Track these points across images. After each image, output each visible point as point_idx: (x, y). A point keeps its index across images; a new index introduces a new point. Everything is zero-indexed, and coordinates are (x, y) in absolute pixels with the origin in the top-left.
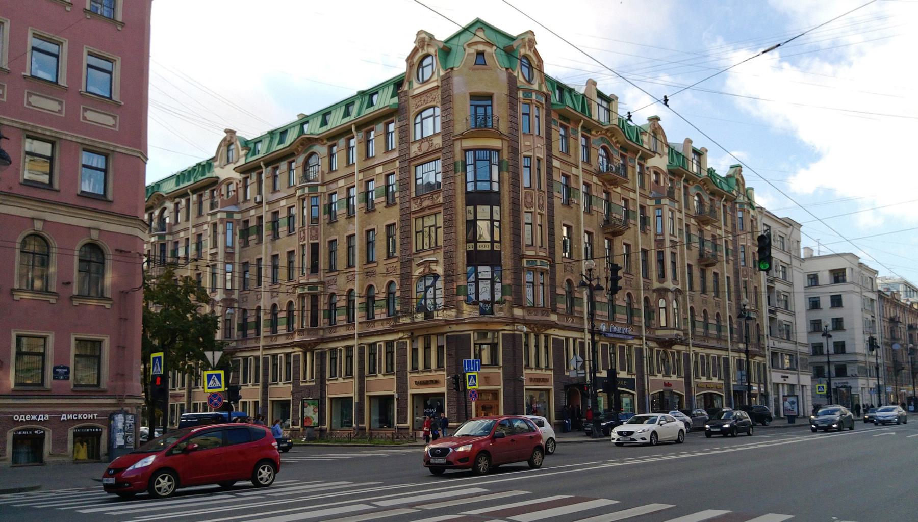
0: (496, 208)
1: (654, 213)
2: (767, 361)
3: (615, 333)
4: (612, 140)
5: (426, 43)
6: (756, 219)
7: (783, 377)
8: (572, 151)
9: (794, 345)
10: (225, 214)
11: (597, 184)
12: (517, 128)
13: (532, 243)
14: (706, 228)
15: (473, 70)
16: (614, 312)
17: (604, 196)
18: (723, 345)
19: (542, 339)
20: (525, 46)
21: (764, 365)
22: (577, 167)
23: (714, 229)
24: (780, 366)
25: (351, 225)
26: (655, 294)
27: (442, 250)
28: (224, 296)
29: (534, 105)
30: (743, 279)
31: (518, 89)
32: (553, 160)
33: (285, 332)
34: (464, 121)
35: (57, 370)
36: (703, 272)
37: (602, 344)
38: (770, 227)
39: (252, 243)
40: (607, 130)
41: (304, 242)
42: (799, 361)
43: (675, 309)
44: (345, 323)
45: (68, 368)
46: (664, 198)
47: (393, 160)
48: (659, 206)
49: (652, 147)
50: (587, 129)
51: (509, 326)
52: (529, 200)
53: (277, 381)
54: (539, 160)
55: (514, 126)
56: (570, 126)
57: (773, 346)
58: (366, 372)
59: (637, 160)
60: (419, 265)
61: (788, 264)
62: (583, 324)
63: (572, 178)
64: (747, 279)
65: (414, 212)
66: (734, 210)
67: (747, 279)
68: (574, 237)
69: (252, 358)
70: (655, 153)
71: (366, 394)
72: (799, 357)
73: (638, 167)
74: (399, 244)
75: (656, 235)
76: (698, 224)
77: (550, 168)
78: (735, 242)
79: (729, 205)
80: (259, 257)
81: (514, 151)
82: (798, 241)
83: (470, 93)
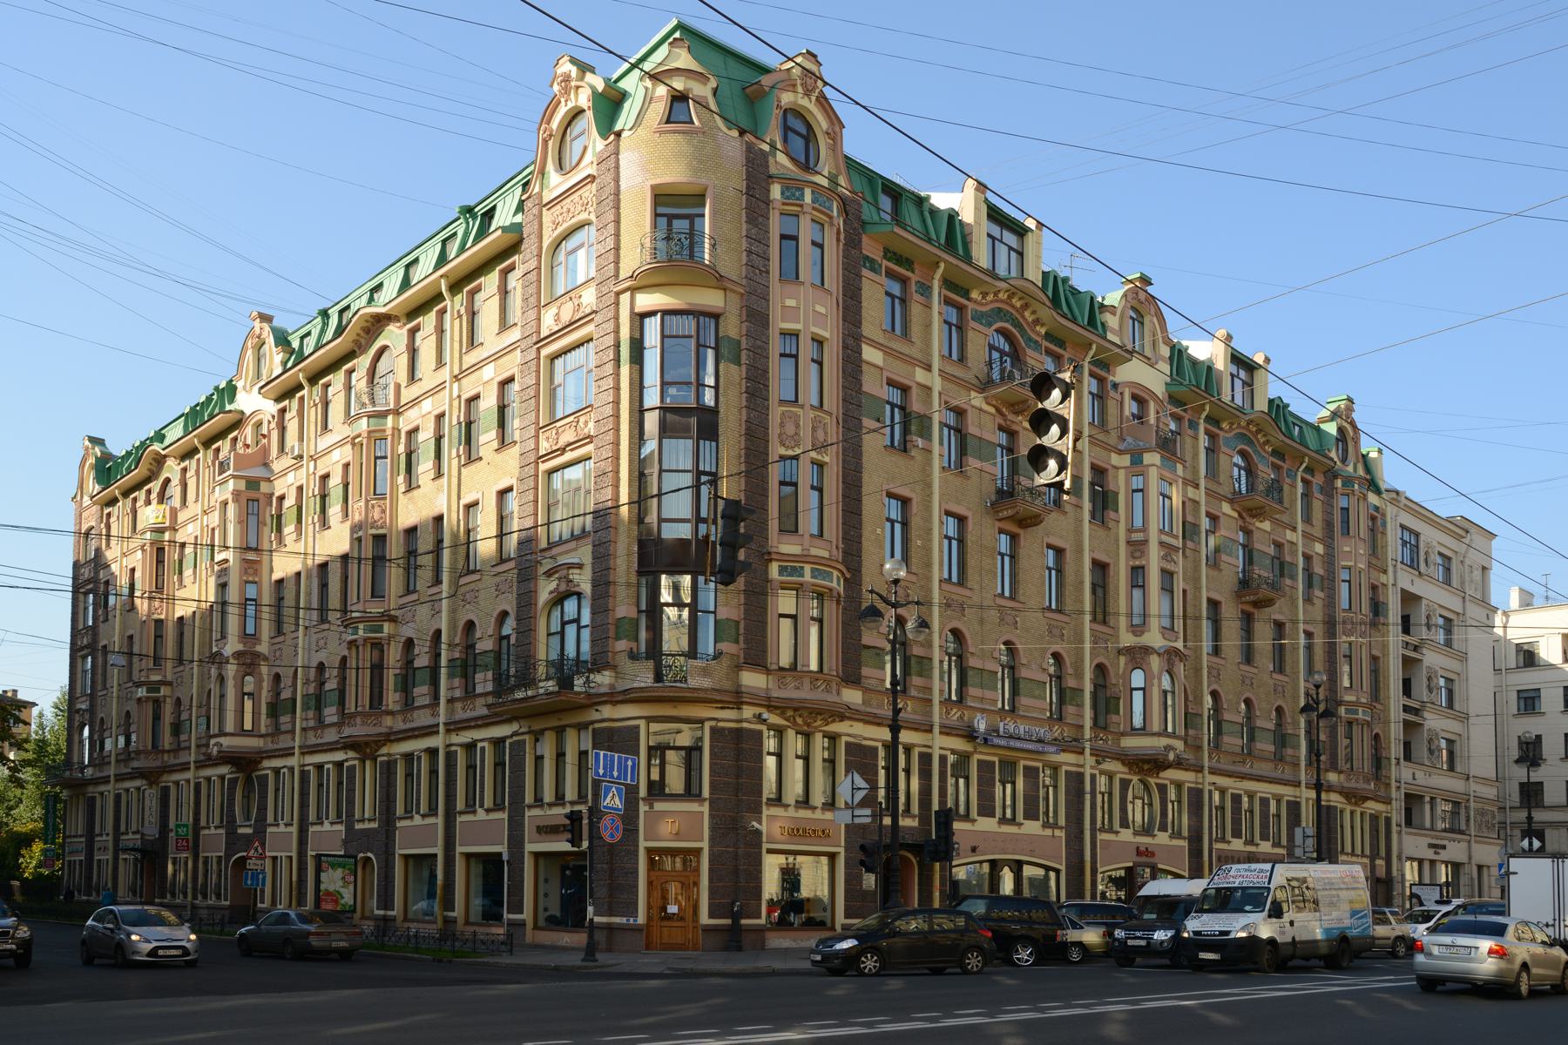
0: (706, 446)
1: (1127, 482)
2: (1394, 812)
3: (1011, 737)
4: (1023, 317)
6: (1384, 515)
7: (1431, 846)
8: (916, 330)
9: (1463, 782)
10: (244, 481)
11: (981, 410)
12: (766, 266)
13: (1351, 684)
15: (661, 133)
16: (1252, 739)
17: (1241, 537)
18: (1287, 773)
19: (819, 742)
20: (794, 86)
21: (1388, 820)
22: (928, 368)
23: (1281, 529)
24: (1428, 824)
26: (1122, 660)
27: (590, 540)
28: (240, 647)
29: (808, 218)
30: (1344, 638)
31: (771, 178)
33: (335, 719)
36: (1248, 620)
37: (978, 760)
38: (1417, 535)
40: (1250, 422)
41: (360, 533)
42: (1472, 813)
43: (1165, 692)
46: (1149, 450)
48: (1138, 469)
49: (1126, 342)
50: (956, 287)
51: (727, 711)
52: (790, 429)
54: (819, 342)
55: (757, 261)
56: (914, 278)
57: (1411, 781)
58: (460, 804)
59: (1299, 474)
60: (549, 574)
61: (1458, 614)
62: (930, 714)
63: (915, 393)
64: (1353, 639)
66: (1328, 491)
67: (1353, 639)
68: (916, 521)
69: (285, 770)
70: (1131, 353)
71: (459, 849)
72: (1472, 804)
73: (1300, 484)
75: (1130, 530)
76: (1240, 515)
77: (852, 365)
78: (1330, 558)
79: (1318, 480)
81: (757, 317)
82: (1484, 568)
83: (653, 187)
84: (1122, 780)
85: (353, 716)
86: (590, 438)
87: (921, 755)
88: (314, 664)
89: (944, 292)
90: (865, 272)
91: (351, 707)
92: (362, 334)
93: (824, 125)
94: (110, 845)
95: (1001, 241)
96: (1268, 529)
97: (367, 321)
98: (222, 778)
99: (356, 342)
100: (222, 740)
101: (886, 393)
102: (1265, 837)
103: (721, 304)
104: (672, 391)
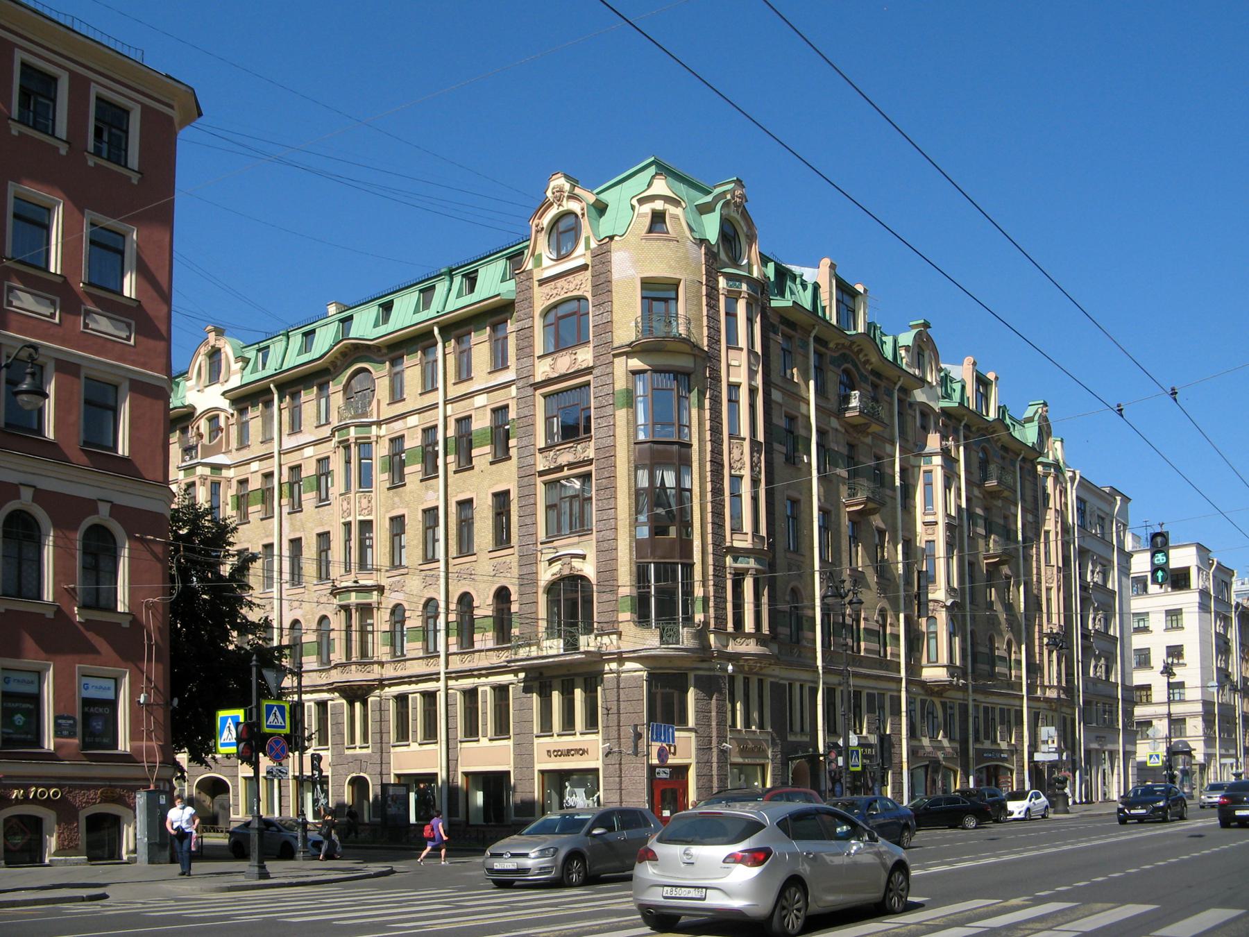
4: (858, 358)
5: (566, 194)
11: (837, 430)
14: (995, 503)
25: (430, 492)
32: (773, 390)
35: (60, 721)
41: (348, 519)
44: (421, 654)
45: (74, 719)
47: (507, 385)
53: (408, 740)
60: (551, 561)
65: (541, 474)
71: (461, 769)
74: (517, 526)
76: (984, 497)
80: (266, 541)
86: (590, 462)
87: (810, 688)
93: (745, 229)
95: (843, 302)
96: (1000, 505)
99: (333, 363)
102: (987, 737)
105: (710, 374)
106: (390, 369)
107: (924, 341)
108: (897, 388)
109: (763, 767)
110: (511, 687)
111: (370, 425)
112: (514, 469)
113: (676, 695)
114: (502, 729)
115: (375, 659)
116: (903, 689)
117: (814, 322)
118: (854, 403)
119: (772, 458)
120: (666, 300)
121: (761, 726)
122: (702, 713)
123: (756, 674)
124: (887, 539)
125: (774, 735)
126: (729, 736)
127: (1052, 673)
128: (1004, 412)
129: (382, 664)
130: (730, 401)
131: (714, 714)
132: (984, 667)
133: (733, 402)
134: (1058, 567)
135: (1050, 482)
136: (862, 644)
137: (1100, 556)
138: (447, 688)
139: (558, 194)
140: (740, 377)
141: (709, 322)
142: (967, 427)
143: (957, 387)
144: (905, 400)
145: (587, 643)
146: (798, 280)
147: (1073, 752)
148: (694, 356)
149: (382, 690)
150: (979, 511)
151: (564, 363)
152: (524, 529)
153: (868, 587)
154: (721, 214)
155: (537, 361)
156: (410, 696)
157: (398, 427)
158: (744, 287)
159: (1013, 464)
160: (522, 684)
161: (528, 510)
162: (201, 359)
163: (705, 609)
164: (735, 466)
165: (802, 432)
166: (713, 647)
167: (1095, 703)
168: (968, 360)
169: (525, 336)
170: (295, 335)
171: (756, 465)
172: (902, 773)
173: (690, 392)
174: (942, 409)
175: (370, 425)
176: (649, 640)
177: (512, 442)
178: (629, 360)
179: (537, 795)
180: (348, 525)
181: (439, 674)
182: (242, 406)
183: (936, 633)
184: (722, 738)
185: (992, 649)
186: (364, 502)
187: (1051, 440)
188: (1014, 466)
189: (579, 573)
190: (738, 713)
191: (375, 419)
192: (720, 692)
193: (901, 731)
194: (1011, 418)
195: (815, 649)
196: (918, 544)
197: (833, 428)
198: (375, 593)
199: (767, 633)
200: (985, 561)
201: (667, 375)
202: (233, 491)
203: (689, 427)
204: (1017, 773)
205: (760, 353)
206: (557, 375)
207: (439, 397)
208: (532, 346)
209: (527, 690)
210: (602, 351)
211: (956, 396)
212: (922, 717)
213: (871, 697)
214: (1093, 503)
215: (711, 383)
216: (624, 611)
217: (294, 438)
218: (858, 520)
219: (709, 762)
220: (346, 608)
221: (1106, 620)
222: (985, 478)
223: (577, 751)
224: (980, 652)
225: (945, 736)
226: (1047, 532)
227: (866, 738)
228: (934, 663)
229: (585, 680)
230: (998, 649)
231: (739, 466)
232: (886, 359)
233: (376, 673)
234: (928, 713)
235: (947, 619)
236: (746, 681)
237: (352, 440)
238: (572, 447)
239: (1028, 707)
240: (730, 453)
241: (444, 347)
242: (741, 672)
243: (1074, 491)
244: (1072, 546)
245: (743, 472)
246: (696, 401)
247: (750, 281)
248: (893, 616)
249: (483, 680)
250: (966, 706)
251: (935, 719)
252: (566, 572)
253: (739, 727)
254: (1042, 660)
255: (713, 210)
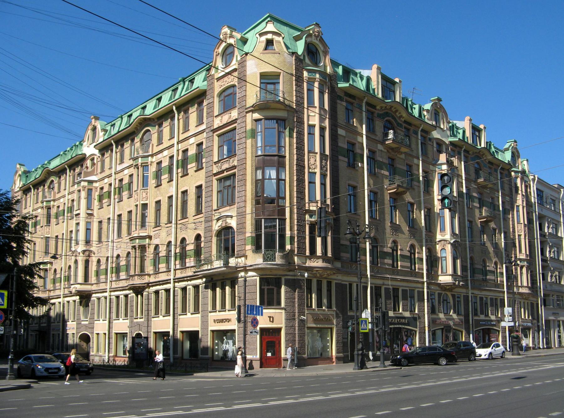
4: (396, 115)
5: (228, 36)
11: (381, 151)
25: (171, 188)
34: (255, 96)
39: (105, 205)
41: (137, 203)
44: (165, 270)
65: (215, 175)
71: (180, 329)
84: (439, 293)
85: (132, 276)
88: (115, 255)
89: (367, 107)
90: (338, 101)
91: (132, 272)
92: (138, 125)
93: (322, 48)
94: (30, 331)
97: (141, 120)
98: (75, 301)
99: (136, 128)
100: (76, 286)
101: (345, 146)
102: (482, 313)
103: (286, 115)
104: (268, 148)
105: (296, 120)
106: (158, 129)
107: (438, 108)
108: (420, 130)
109: (331, 329)
110: (200, 286)
111: (148, 156)
112: (204, 173)
113: (275, 289)
114: (196, 310)
115: (146, 273)
116: (425, 287)
117: (364, 95)
118: (391, 136)
119: (338, 164)
120: (274, 84)
121: (329, 307)
122: (290, 300)
123: (326, 278)
124: (415, 208)
125: (338, 312)
126: (306, 312)
127: (524, 279)
128: (490, 145)
129: (149, 275)
130: (309, 134)
131: (296, 300)
132: (480, 277)
133: (311, 134)
134: (524, 224)
135: (519, 181)
136: (399, 263)
137: (553, 219)
138: (174, 287)
139: (225, 36)
140: (315, 121)
141: (296, 93)
142: (465, 151)
143: (461, 131)
144: (426, 137)
145: (232, 262)
146: (358, 75)
147: (538, 321)
148: (288, 110)
149: (149, 288)
150: (475, 194)
151: (226, 119)
152: (207, 204)
153: (403, 233)
154: (306, 41)
155: (215, 118)
156: (160, 291)
157: (160, 156)
158: (318, 76)
159: (496, 171)
160: (204, 285)
161: (209, 194)
162: (90, 132)
163: (292, 243)
164: (311, 167)
165: (358, 151)
166: (296, 263)
167: (551, 295)
168: (467, 118)
169: (211, 106)
170: (125, 117)
171: (324, 167)
172: (425, 333)
173: (285, 129)
174: (450, 142)
175: (148, 156)
176: (256, 260)
177: (204, 160)
178: (253, 114)
179: (209, 344)
180: (137, 206)
181: (170, 280)
182: (103, 152)
183: (446, 257)
184: (301, 313)
185: (485, 266)
186: (144, 194)
187: (520, 160)
188: (497, 172)
189: (230, 225)
190: (313, 300)
191: (150, 153)
192: (300, 287)
193: (424, 310)
194: (495, 147)
195: (366, 265)
196: (435, 211)
197: (379, 150)
198: (147, 239)
199: (330, 256)
200: (479, 221)
201: (273, 121)
202: (97, 193)
203: (285, 147)
204: (502, 332)
205: (327, 109)
206: (222, 124)
207: (175, 141)
208: (213, 111)
209: (206, 287)
210: (241, 110)
211: (460, 136)
212: (439, 302)
213: (404, 292)
214: (546, 192)
215: (297, 124)
216: (248, 245)
217: (121, 165)
218: (396, 197)
219: (293, 326)
220: (134, 247)
221: (558, 252)
222: (478, 177)
223: (226, 320)
224: (476, 268)
225: (454, 312)
226: (518, 206)
227: (401, 313)
228: (445, 274)
229: (231, 281)
230: (488, 266)
231: (314, 167)
232: (414, 116)
233: (146, 280)
234: (444, 300)
235: (451, 249)
236: (319, 283)
237: (140, 164)
238: (228, 160)
239: (507, 297)
240: (309, 161)
241: (179, 116)
242: (315, 277)
243: (535, 186)
244: (534, 214)
245: (316, 170)
246: (288, 134)
247: (323, 74)
248: (419, 248)
249: (189, 283)
250: (468, 296)
251: (448, 304)
252: (224, 225)
253: (314, 307)
254: (516, 273)
255: (302, 39)
